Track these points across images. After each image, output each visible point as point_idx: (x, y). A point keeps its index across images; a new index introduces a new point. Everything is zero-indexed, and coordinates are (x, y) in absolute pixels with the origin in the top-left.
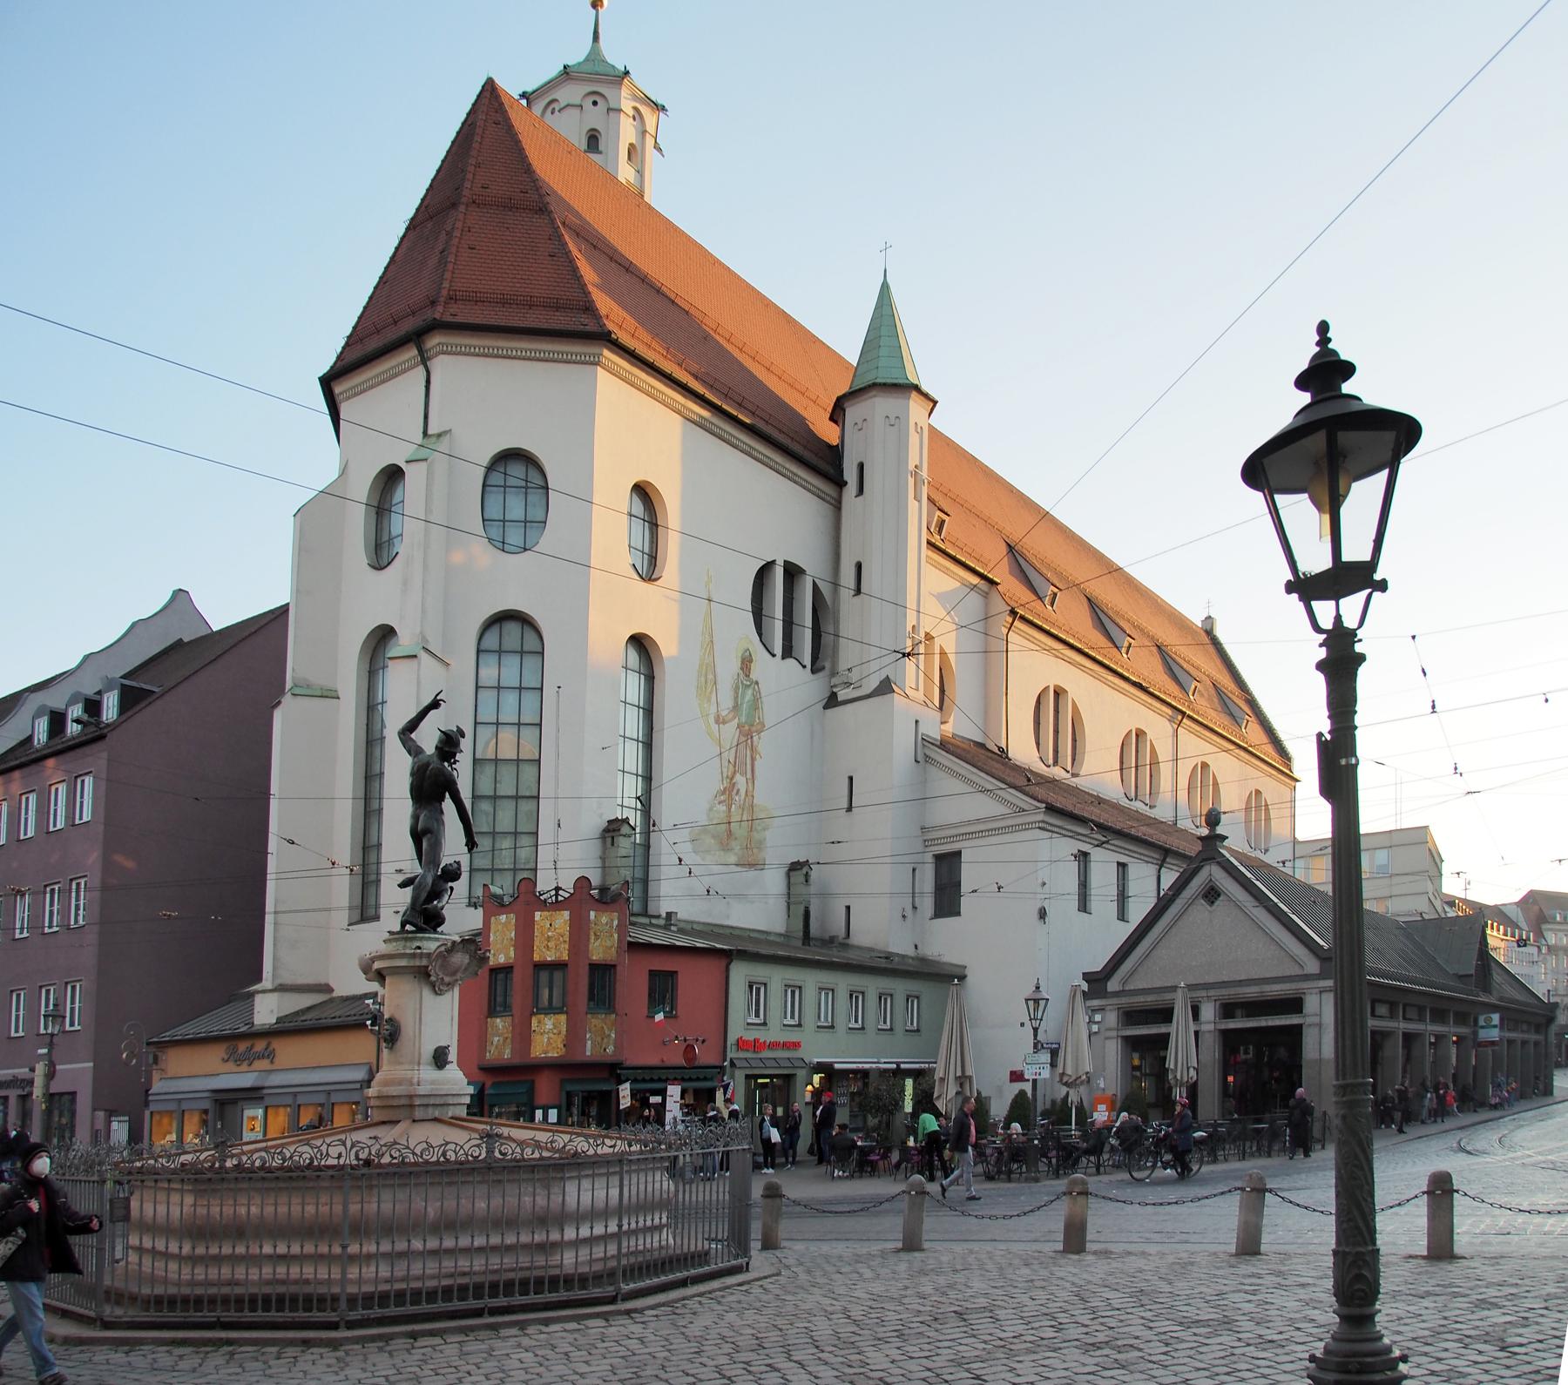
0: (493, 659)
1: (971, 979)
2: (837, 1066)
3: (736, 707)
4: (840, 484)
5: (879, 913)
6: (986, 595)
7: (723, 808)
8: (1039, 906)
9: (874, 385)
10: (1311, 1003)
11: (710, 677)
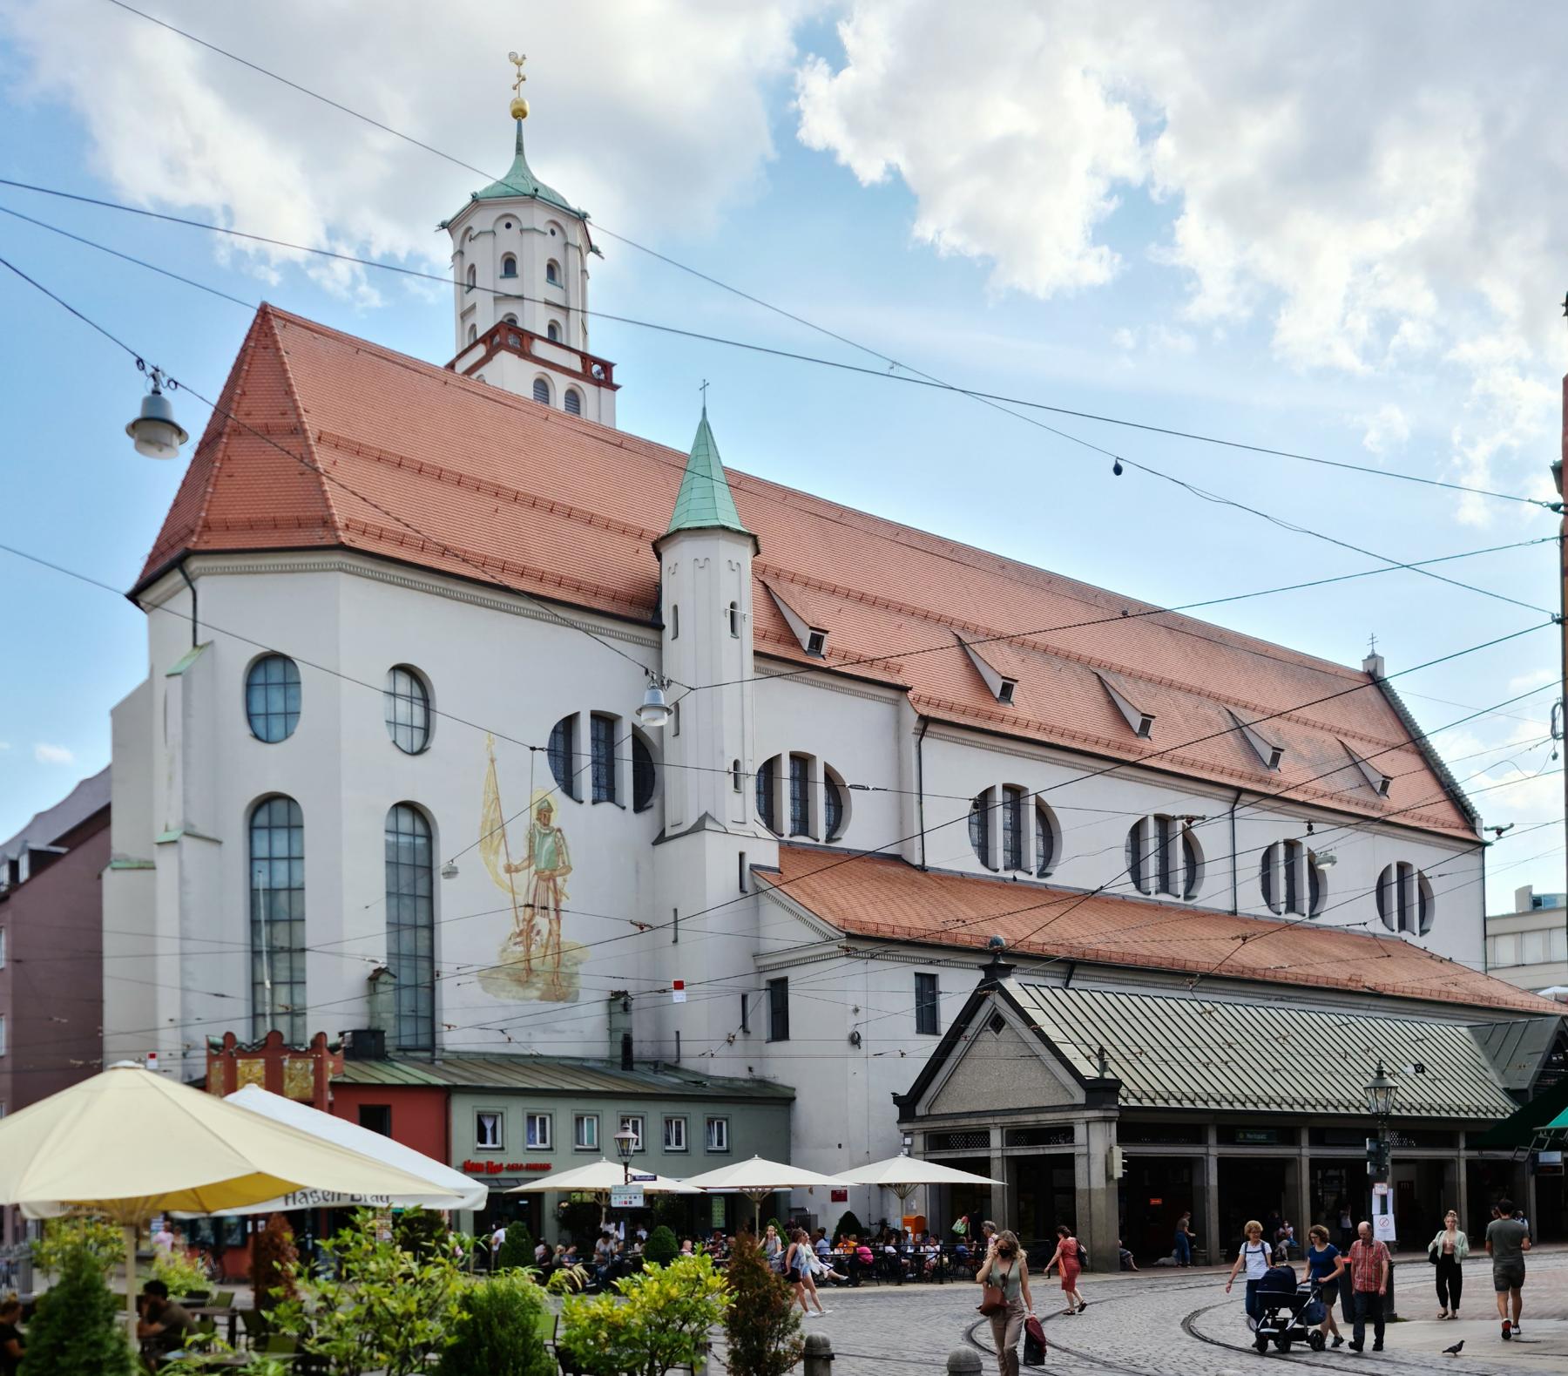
0: (265, 833)
1: (801, 1101)
2: (1118, 1173)
3: (532, 856)
5: (705, 1034)
6: (896, 703)
7: (520, 948)
8: (850, 1031)
9: (679, 530)
10: (1080, 1132)
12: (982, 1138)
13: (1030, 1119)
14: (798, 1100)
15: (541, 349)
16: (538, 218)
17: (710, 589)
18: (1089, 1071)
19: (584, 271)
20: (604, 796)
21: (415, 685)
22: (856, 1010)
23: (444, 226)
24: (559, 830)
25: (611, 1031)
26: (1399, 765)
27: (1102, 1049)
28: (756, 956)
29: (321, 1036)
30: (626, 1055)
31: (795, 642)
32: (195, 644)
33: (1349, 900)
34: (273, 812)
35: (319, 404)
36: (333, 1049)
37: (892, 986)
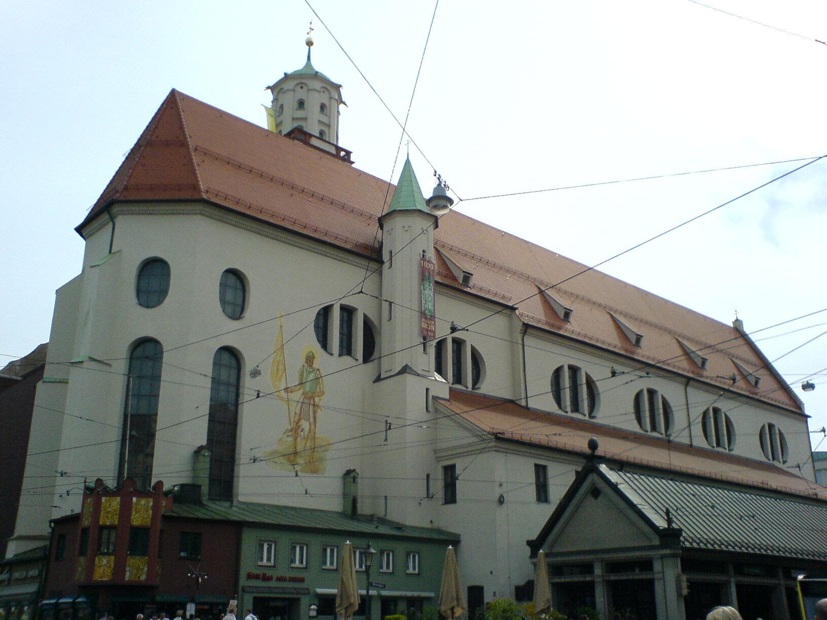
2: (685, 592)
4: (381, 262)
6: (510, 316)
7: (290, 439)
9: (394, 211)
10: (657, 566)
11: (281, 367)
12: (587, 568)
13: (622, 556)
14: (462, 543)
15: (314, 142)
16: (317, 85)
17: (408, 246)
18: (661, 523)
19: (338, 112)
20: (345, 351)
21: (238, 281)
22: (501, 485)
23: (268, 88)
24: (318, 370)
25: (345, 495)
26: (762, 374)
27: (667, 509)
28: (435, 451)
29: (160, 484)
30: (352, 511)
31: (455, 279)
32: (110, 252)
33: (747, 445)
34: (146, 354)
35: (194, 134)
36: (166, 494)
37: (518, 472)
